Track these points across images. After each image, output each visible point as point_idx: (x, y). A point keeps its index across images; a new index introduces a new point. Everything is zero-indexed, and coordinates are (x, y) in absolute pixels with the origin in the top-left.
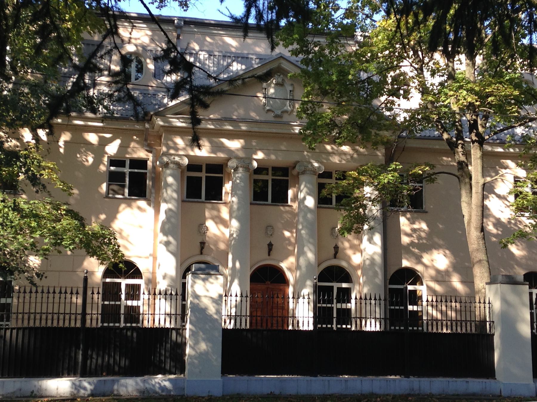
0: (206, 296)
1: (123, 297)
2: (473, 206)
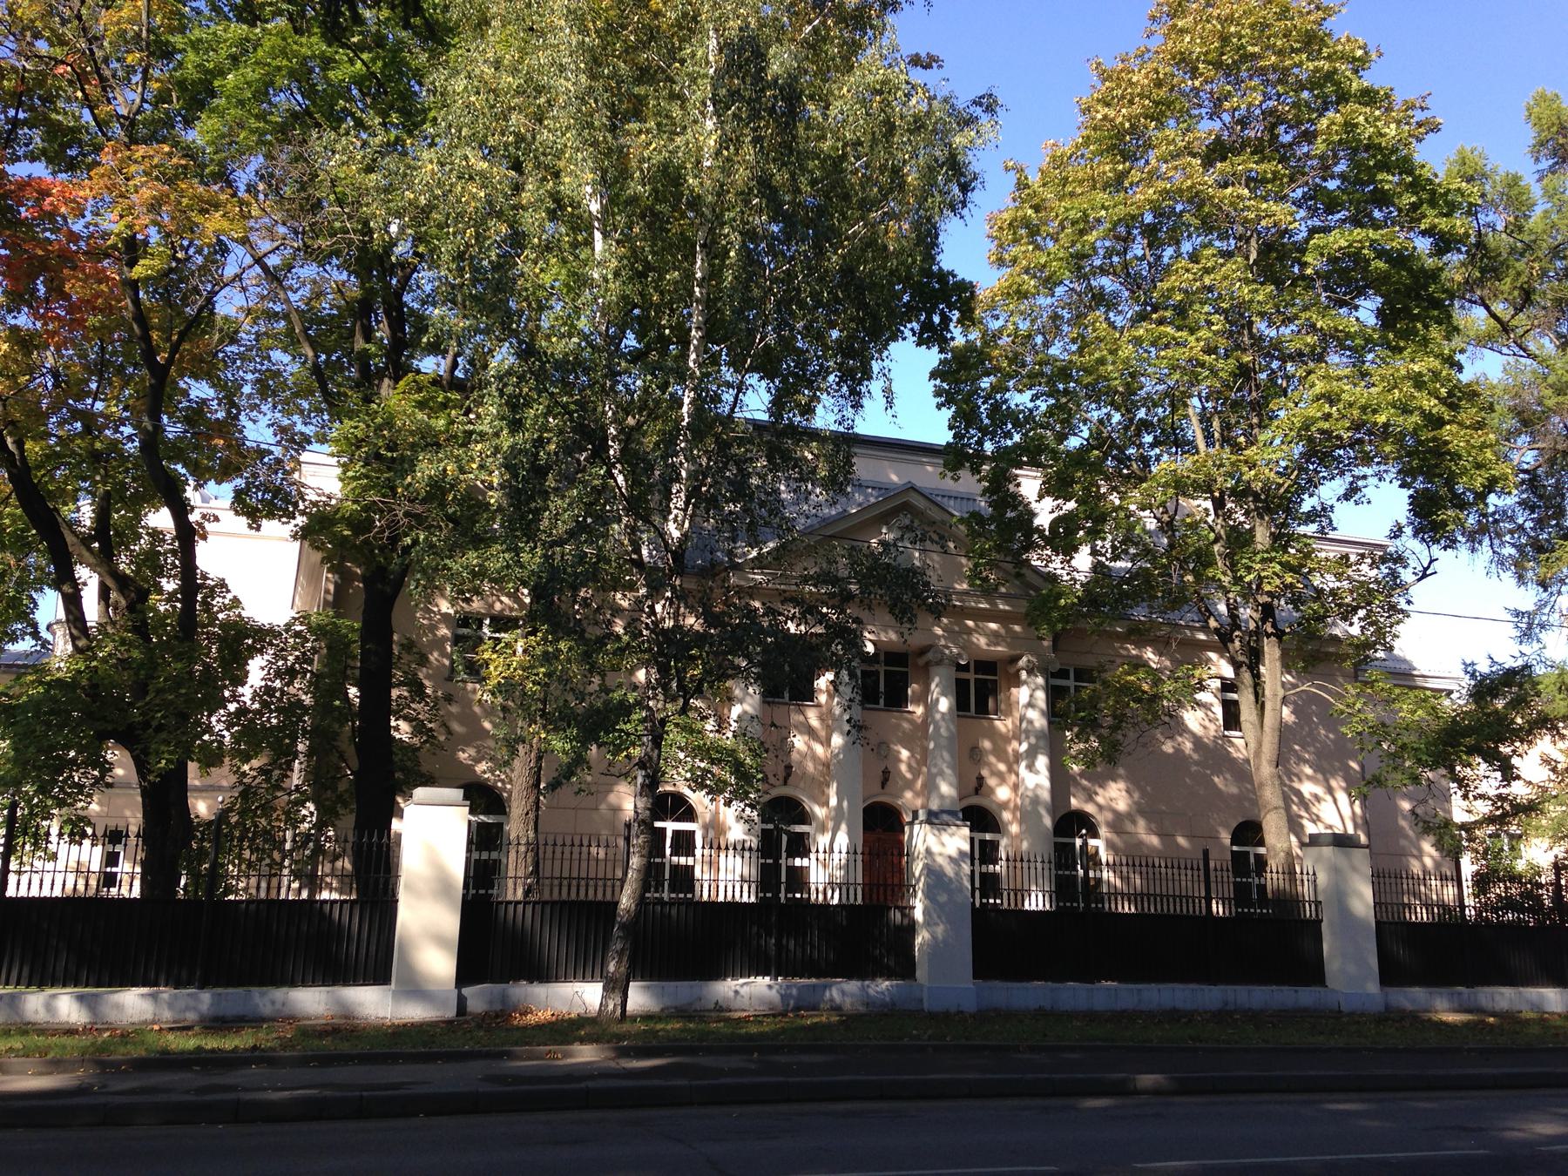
0: (941, 854)
1: (668, 851)
2: (1266, 728)
